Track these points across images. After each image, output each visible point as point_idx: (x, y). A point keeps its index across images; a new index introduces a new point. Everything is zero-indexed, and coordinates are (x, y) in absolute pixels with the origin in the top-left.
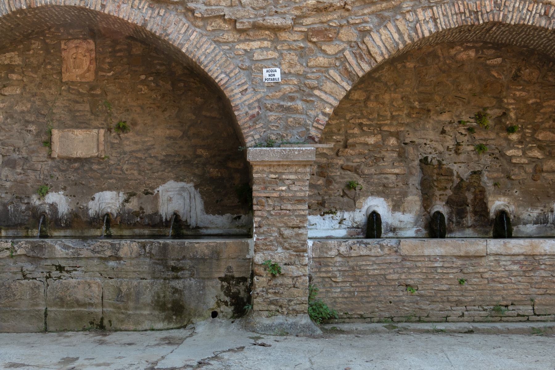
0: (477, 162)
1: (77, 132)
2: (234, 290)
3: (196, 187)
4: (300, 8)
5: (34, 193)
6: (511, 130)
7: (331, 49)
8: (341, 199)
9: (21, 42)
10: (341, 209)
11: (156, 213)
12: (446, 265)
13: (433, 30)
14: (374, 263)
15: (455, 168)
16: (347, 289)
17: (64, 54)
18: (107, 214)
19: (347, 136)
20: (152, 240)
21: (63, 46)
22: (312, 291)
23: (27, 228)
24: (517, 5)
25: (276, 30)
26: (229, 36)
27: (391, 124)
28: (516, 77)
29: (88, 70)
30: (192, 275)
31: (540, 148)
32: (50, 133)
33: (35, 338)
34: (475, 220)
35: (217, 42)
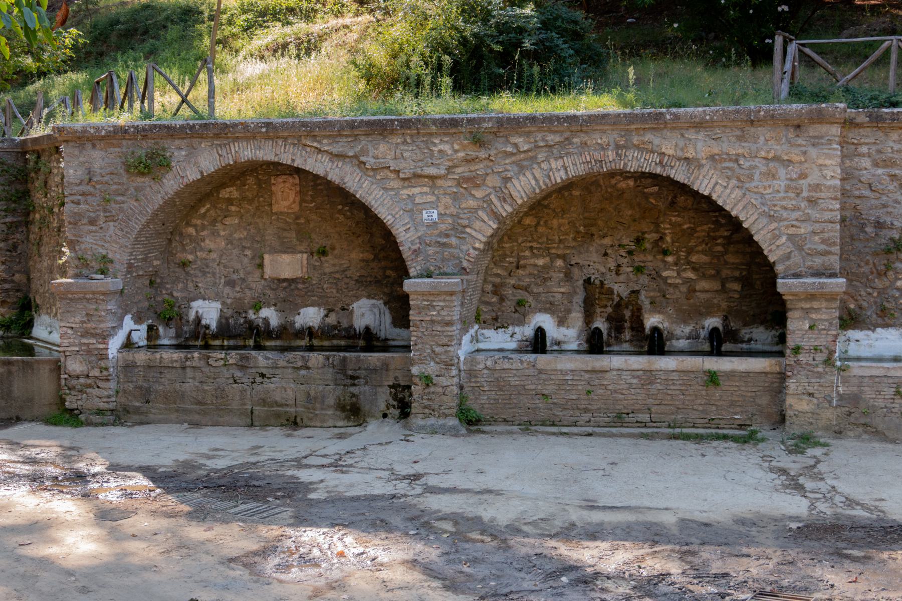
0: (636, 282)
1: (285, 256)
2: (400, 396)
3: (385, 304)
4: (452, 160)
5: (250, 308)
6: (665, 253)
7: (479, 194)
8: (513, 315)
9: (238, 178)
10: (512, 324)
11: (351, 327)
12: (576, 378)
13: (564, 177)
14: (515, 375)
15: (616, 288)
16: (493, 397)
17: (273, 188)
18: (310, 328)
19: (519, 258)
20: (334, 353)
21: (273, 181)
22: (462, 399)
23: (245, 339)
24: (636, 155)
25: (433, 178)
26: (395, 184)
27: (558, 248)
28: (673, 203)
29: (294, 202)
30: (366, 383)
31: (694, 269)
32: (262, 258)
33: (241, 430)
34: (632, 336)
35: (385, 189)
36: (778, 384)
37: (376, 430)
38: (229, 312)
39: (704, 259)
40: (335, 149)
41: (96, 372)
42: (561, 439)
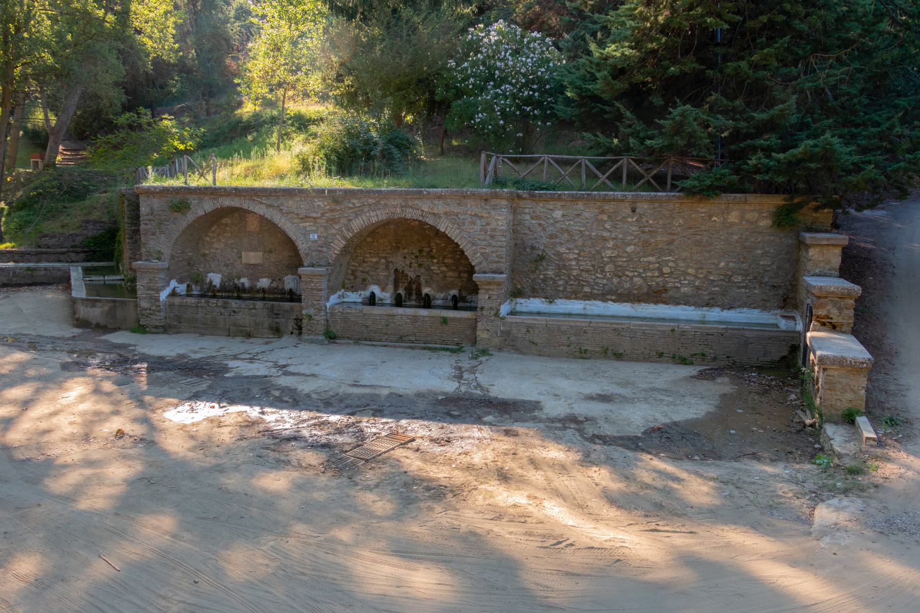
6: (433, 257)
7: (337, 227)
19: (364, 257)
22: (328, 326)
25: (315, 218)
31: (446, 266)
36: (473, 326)
37: (286, 340)
38: (225, 280)
39: (451, 261)
40: (268, 202)
41: (154, 308)
42: (370, 348)
